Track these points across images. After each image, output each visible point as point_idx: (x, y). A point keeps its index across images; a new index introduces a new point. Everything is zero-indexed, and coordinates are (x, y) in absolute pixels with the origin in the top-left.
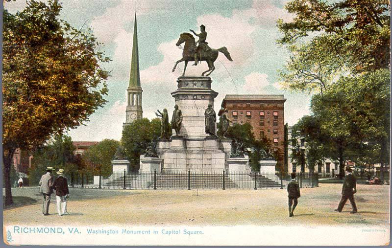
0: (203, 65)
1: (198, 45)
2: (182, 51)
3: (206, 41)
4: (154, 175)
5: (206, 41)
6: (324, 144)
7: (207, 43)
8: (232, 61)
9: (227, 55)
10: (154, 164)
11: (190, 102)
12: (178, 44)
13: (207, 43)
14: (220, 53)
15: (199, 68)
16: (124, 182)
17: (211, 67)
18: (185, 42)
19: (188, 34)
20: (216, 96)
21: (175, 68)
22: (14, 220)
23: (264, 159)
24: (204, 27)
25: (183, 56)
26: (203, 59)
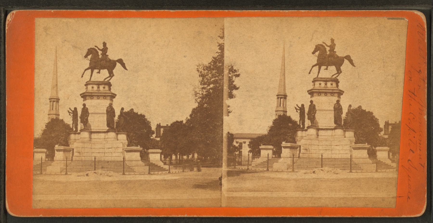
0: (333, 69)
1: (100, 57)
2: (316, 58)
3: (335, 50)
4: (65, 162)
5: (335, 50)
6: (160, 141)
7: (108, 56)
8: (355, 66)
9: (123, 65)
10: (66, 153)
11: (323, 98)
13: (108, 56)
14: (345, 60)
15: (329, 72)
16: (268, 164)
17: (111, 75)
18: (319, 51)
19: (93, 49)
21: (311, 71)
23: (379, 146)
24: (334, 40)
25: (90, 65)
26: (104, 68)
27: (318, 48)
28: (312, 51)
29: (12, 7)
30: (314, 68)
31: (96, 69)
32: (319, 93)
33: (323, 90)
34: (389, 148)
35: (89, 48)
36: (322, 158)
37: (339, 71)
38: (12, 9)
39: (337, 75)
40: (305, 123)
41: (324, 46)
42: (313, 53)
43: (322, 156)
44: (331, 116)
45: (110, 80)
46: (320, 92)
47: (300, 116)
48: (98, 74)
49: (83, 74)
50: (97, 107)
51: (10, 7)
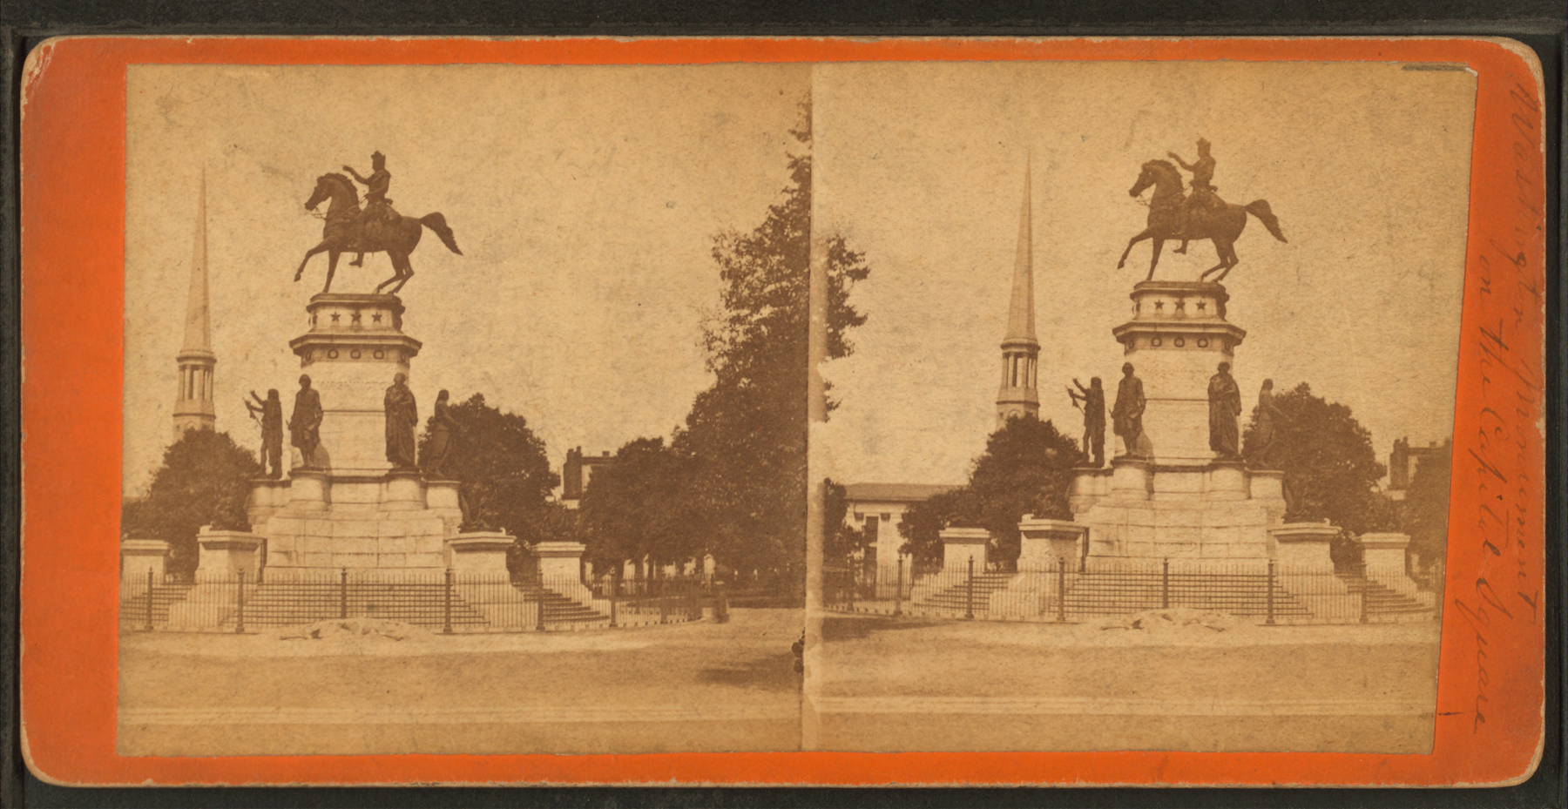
0: (1204, 251)
1: (363, 207)
3: (387, 196)
4: (237, 587)
5: (387, 196)
6: (582, 509)
7: (390, 202)
8: (1285, 241)
9: (446, 236)
11: (1170, 357)
12: (311, 205)
13: (390, 202)
14: (1250, 217)
15: (1190, 261)
16: (969, 596)
17: (403, 271)
18: (1154, 187)
19: (337, 176)
20: (414, 353)
22: (104, 701)
23: (1374, 530)
25: (325, 236)
26: (376, 247)
27: (1152, 174)
28: (1131, 186)
29: (44, 27)
30: (1138, 245)
31: (346, 250)
32: (1157, 337)
33: (356, 337)
34: (1407, 539)
35: (323, 174)
36: (1166, 575)
37: (1228, 259)
38: (42, 33)
39: (1222, 271)
40: (1106, 447)
41: (1174, 168)
42: (1135, 192)
43: (1166, 565)
44: (1199, 420)
45: (397, 289)
46: (1159, 335)
47: (1088, 422)
48: (356, 268)
49: (301, 270)
50: (351, 387)
51: (35, 24)
